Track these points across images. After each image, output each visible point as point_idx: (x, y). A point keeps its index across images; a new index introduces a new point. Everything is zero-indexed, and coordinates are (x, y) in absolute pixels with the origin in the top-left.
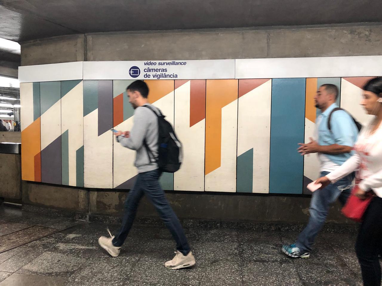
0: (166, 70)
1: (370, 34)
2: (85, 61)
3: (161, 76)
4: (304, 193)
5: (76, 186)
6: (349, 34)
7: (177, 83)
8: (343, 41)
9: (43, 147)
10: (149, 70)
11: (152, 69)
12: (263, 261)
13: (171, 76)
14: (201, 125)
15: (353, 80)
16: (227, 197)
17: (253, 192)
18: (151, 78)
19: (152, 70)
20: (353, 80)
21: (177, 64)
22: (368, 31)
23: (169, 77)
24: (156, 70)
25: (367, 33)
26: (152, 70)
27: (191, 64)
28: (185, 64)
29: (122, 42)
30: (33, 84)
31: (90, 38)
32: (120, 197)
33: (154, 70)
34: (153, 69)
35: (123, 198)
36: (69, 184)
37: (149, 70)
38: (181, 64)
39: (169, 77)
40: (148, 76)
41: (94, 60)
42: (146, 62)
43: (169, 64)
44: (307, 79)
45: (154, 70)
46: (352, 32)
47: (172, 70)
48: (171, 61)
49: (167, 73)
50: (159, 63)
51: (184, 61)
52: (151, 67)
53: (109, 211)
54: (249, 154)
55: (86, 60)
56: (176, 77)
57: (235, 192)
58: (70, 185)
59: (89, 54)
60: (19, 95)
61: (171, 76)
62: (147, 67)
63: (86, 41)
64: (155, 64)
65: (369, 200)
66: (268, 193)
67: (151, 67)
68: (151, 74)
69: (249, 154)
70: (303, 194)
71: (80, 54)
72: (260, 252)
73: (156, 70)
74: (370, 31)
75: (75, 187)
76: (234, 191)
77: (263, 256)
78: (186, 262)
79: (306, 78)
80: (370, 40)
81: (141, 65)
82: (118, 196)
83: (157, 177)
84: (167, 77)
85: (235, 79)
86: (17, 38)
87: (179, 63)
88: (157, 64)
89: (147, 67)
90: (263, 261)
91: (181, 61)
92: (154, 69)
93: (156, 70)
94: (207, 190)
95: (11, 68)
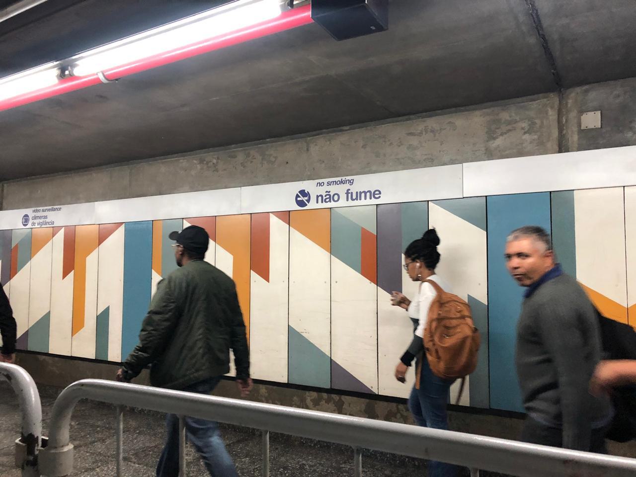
0: (46, 217)
1: (217, 163)
2: (560, 151)
4: (332, 387)
5: (468, 405)
6: (198, 164)
8: (193, 173)
13: (50, 223)
14: (71, 275)
17: (109, 360)
22: (215, 159)
25: (215, 161)
27: (65, 208)
36: (27, 349)
42: (33, 209)
43: (49, 210)
44: (429, 202)
46: (201, 161)
48: (50, 207)
49: (47, 220)
50: (328, 183)
54: (106, 312)
57: (287, 382)
58: (50, 352)
61: (50, 223)
64: (322, 184)
65: (547, 424)
66: (120, 362)
69: (106, 312)
70: (331, 389)
74: (218, 158)
75: (468, 407)
76: (284, 380)
79: (550, 192)
80: (217, 170)
82: (135, 377)
84: (360, 199)
85: (463, 198)
87: (348, 181)
88: (326, 184)
94: (494, 407)
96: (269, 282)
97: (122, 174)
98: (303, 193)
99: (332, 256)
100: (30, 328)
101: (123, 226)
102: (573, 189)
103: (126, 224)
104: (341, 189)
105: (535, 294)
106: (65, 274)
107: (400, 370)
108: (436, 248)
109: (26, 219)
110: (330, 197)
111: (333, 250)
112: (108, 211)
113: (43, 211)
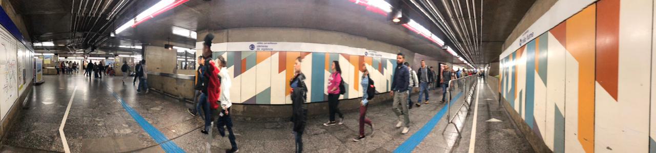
0: (267, 46)
3: (265, 49)
7: (273, 53)
9: (285, 71)
10: (259, 46)
12: (316, 134)
16: (281, 106)
18: (261, 50)
21: (272, 44)
28: (276, 43)
29: (245, 32)
31: (230, 31)
32: (244, 107)
35: (245, 108)
36: (366, 84)
37: (259, 46)
40: (259, 49)
41: (232, 41)
43: (269, 43)
47: (270, 46)
52: (260, 45)
53: (238, 114)
55: (228, 41)
59: (230, 39)
60: (216, 52)
62: (258, 45)
63: (228, 33)
67: (260, 45)
68: (261, 48)
71: (225, 38)
72: (313, 130)
73: (263, 46)
77: (315, 132)
81: (255, 44)
86: (195, 30)
89: (258, 45)
90: (316, 134)
96: (235, 77)
97: (308, 33)
98: (366, 52)
99: (596, 82)
100: (258, 94)
101: (278, 53)
102: (648, 138)
103: (279, 51)
104: (375, 53)
105: (52, 94)
106: (280, 71)
107: (497, 63)
108: (50, 41)
109: (252, 47)
110: (373, 55)
111: (373, 66)
112: (305, 47)
113: (265, 43)
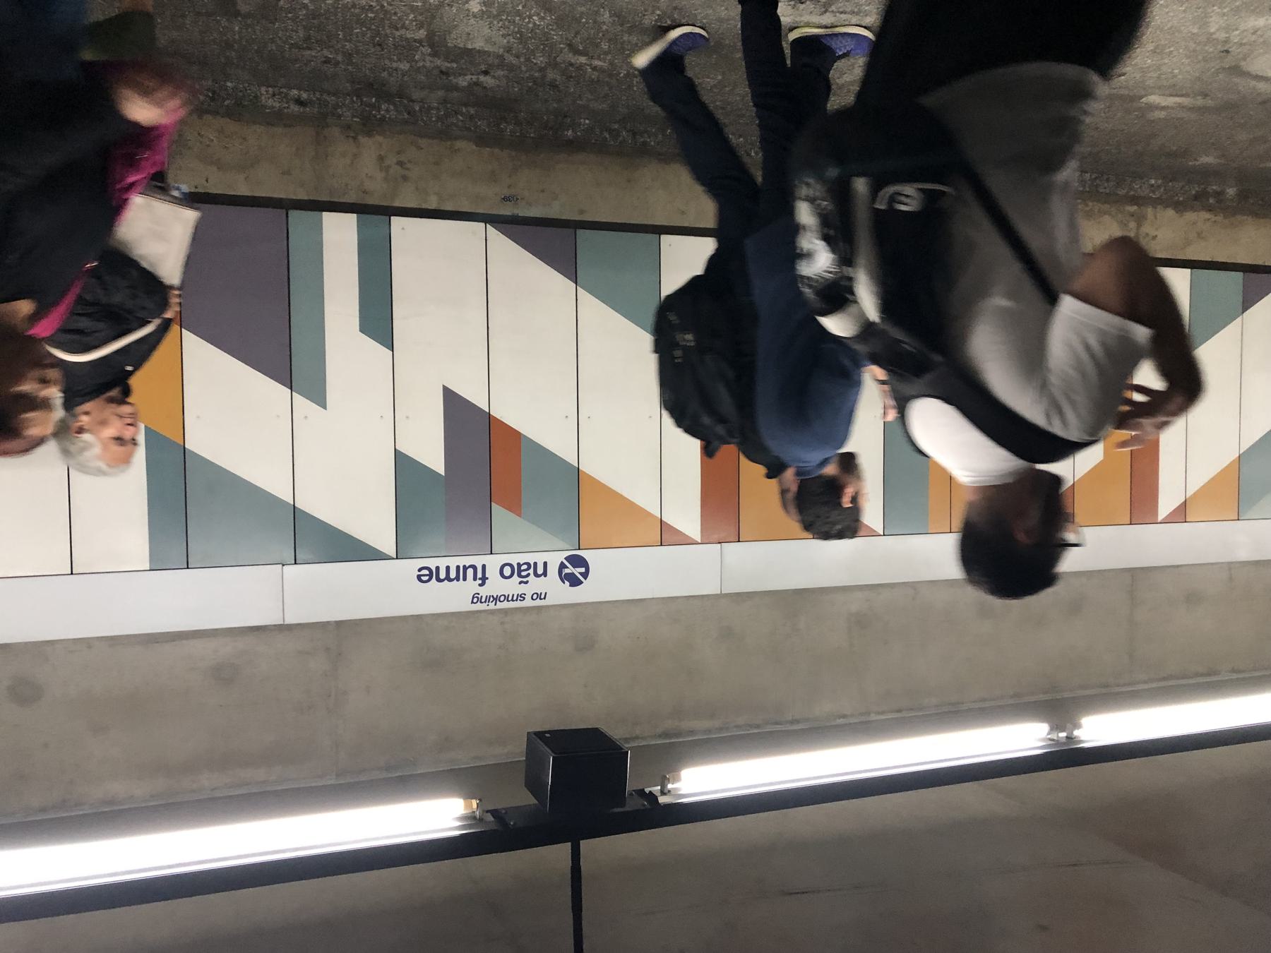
11: (451, 580)
15: (874, 534)
19: (453, 575)
20: (874, 534)
23: (438, 568)
24: (431, 576)
26: (453, 575)
30: (834, 52)
33: (443, 575)
34: (448, 578)
38: (507, 598)
39: (438, 568)
45: (443, 575)
51: (479, 607)
56: (524, 567)
78: (1163, 108)
83: (861, 714)
84: (458, 567)
91: (505, 605)
92: (439, 580)
93: (431, 576)
95: (857, 393)
